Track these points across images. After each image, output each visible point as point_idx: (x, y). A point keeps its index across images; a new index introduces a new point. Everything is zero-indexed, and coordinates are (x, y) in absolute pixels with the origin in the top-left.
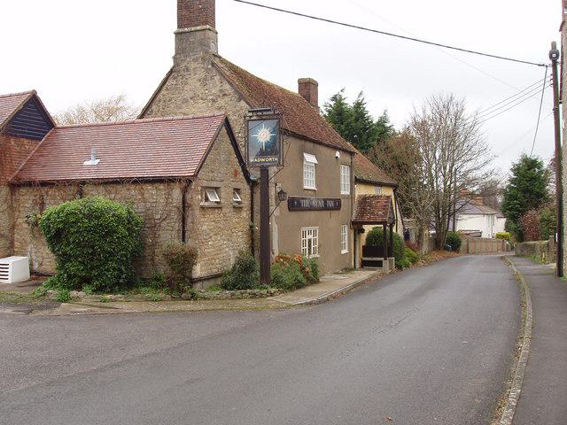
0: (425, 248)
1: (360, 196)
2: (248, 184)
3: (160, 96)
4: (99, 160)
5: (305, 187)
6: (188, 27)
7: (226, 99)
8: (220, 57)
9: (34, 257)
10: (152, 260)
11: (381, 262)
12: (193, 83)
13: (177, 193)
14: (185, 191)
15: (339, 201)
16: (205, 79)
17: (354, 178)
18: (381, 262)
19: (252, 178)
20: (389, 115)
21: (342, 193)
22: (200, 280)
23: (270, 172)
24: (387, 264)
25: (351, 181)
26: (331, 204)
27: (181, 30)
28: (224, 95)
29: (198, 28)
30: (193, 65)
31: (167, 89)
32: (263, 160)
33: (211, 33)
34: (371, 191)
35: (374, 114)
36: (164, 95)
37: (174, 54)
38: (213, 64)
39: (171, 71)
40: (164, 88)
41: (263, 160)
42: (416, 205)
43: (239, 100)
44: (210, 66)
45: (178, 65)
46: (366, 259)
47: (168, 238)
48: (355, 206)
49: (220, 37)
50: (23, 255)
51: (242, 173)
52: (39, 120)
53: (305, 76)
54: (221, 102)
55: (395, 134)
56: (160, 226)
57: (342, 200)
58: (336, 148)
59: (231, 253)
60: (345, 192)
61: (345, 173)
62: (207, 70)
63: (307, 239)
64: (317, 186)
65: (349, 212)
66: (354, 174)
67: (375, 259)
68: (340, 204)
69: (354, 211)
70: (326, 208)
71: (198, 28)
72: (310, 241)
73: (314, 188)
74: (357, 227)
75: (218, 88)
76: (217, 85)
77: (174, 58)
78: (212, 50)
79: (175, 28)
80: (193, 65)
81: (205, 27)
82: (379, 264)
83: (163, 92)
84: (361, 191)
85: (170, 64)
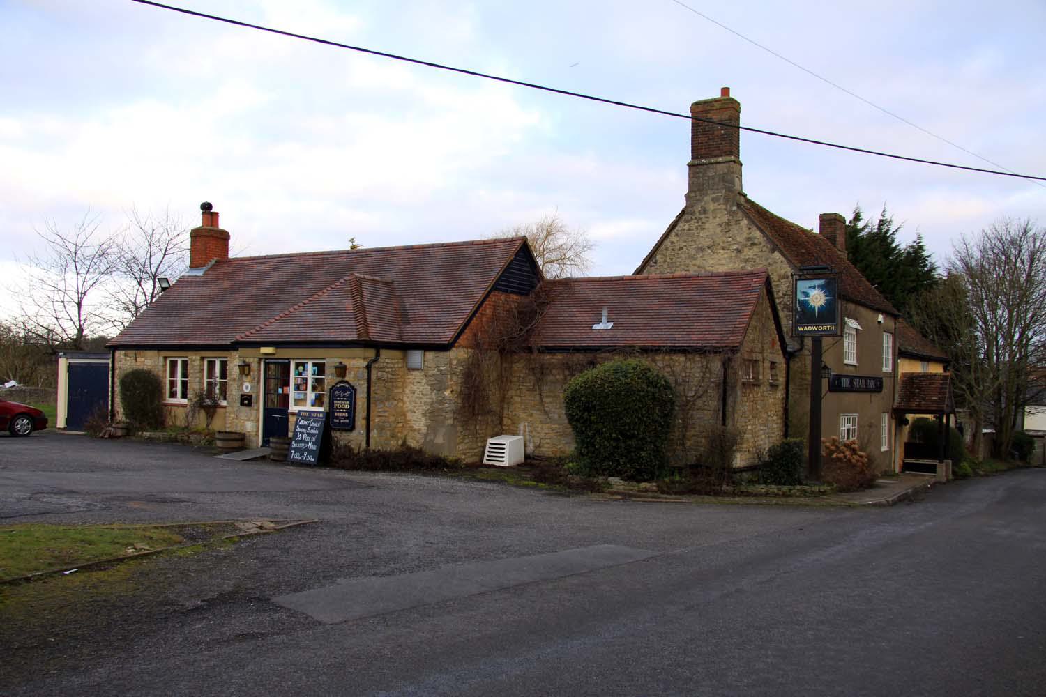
0: (982, 453)
1: (904, 375)
2: (784, 357)
3: (667, 243)
4: (612, 324)
5: (846, 361)
6: (705, 158)
7: (755, 249)
8: (745, 196)
9: (528, 437)
10: (683, 444)
11: (935, 466)
12: (712, 226)
13: (716, 365)
14: (726, 364)
15: (880, 380)
16: (728, 224)
17: (897, 351)
18: (935, 466)
19: (789, 350)
20: (860, 205)
21: (884, 369)
22: (742, 470)
23: (823, 344)
24: (944, 469)
25: (894, 355)
26: (872, 384)
27: (697, 162)
28: (753, 244)
29: (720, 159)
30: (712, 206)
31: (677, 235)
32: (815, 328)
33: (736, 166)
34: (917, 368)
35: (903, 241)
36: (672, 243)
37: (687, 191)
38: (738, 205)
39: (683, 213)
40: (673, 234)
41: (815, 328)
42: (970, 386)
43: (773, 251)
44: (735, 208)
45: (692, 206)
46: (907, 461)
47: (704, 417)
48: (898, 388)
49: (745, 170)
50: (514, 434)
51: (778, 343)
52: (528, 272)
53: (830, 210)
54: (748, 253)
55: (899, 254)
56: (694, 404)
57: (884, 379)
58: (879, 311)
59: (767, 441)
60: (887, 368)
61: (887, 342)
62: (731, 213)
63: (846, 428)
64: (858, 361)
65: (892, 395)
66: (898, 345)
67: (921, 462)
68: (881, 387)
69: (897, 396)
70: (866, 390)
71: (720, 159)
72: (848, 430)
73: (854, 362)
74: (898, 417)
75: (745, 235)
76: (744, 229)
77: (687, 196)
78: (737, 187)
79: (689, 159)
80: (712, 206)
81: (728, 158)
82: (932, 469)
83: (672, 238)
84: (906, 367)
85: (682, 204)
